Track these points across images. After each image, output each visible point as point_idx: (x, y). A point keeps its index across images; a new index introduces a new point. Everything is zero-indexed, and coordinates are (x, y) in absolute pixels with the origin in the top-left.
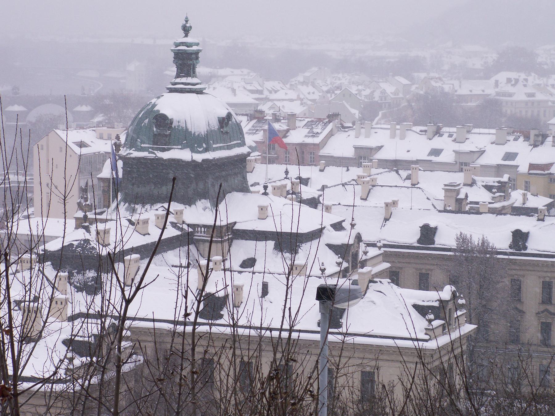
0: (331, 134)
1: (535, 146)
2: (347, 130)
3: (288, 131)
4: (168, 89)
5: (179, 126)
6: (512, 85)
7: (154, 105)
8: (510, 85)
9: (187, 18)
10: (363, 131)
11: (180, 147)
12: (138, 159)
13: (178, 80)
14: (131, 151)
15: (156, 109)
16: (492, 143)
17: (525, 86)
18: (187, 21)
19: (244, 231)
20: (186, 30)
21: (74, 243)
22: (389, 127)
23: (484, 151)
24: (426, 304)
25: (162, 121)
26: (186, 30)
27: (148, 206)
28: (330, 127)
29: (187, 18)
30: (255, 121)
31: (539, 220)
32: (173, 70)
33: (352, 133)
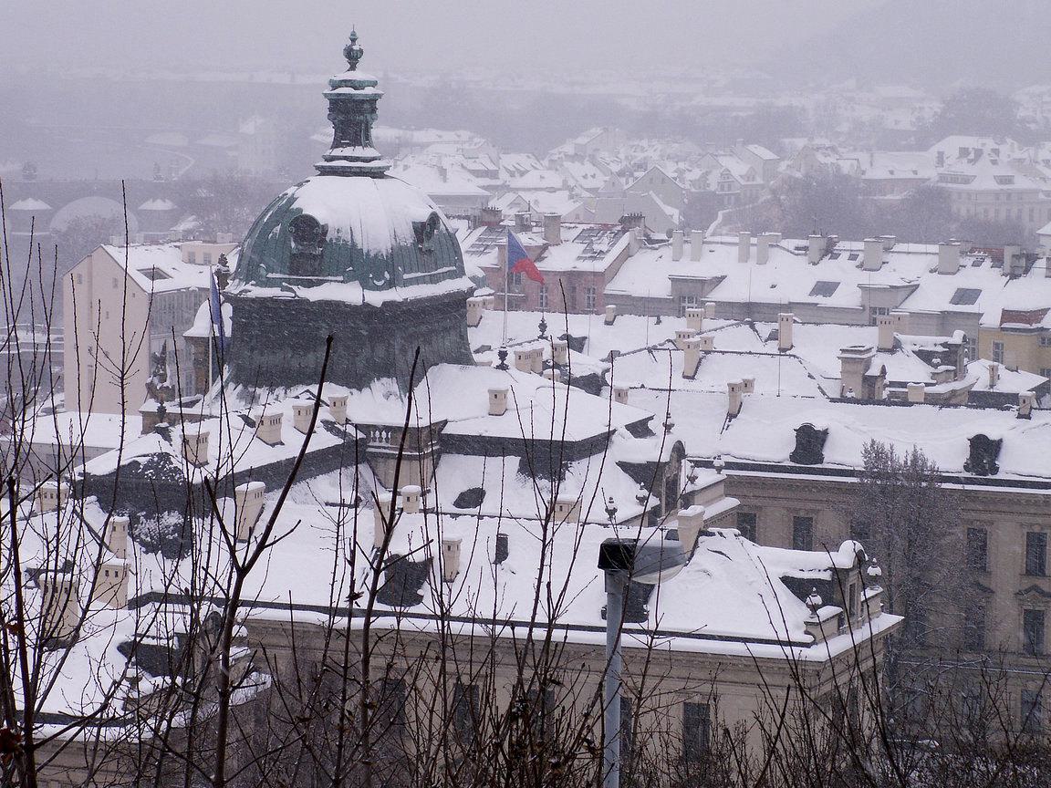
0: (626, 254)
1: (1014, 276)
2: (657, 246)
3: (545, 248)
4: (317, 168)
5: (338, 239)
6: (970, 161)
7: (293, 200)
8: (965, 160)
9: (353, 34)
10: (687, 247)
11: (341, 278)
12: (262, 302)
13: (337, 152)
14: (248, 287)
15: (294, 206)
16: (931, 271)
17: (994, 162)
18: (353, 40)
19: (462, 438)
20: (353, 57)
21: (139, 459)
22: (736, 240)
23: (917, 286)
24: (806, 575)
25: (307, 228)
26: (353, 57)
27: (280, 391)
28: (625, 240)
29: (353, 34)
30: (483, 229)
31: (1020, 416)
32: (329, 132)
33: (667, 252)
